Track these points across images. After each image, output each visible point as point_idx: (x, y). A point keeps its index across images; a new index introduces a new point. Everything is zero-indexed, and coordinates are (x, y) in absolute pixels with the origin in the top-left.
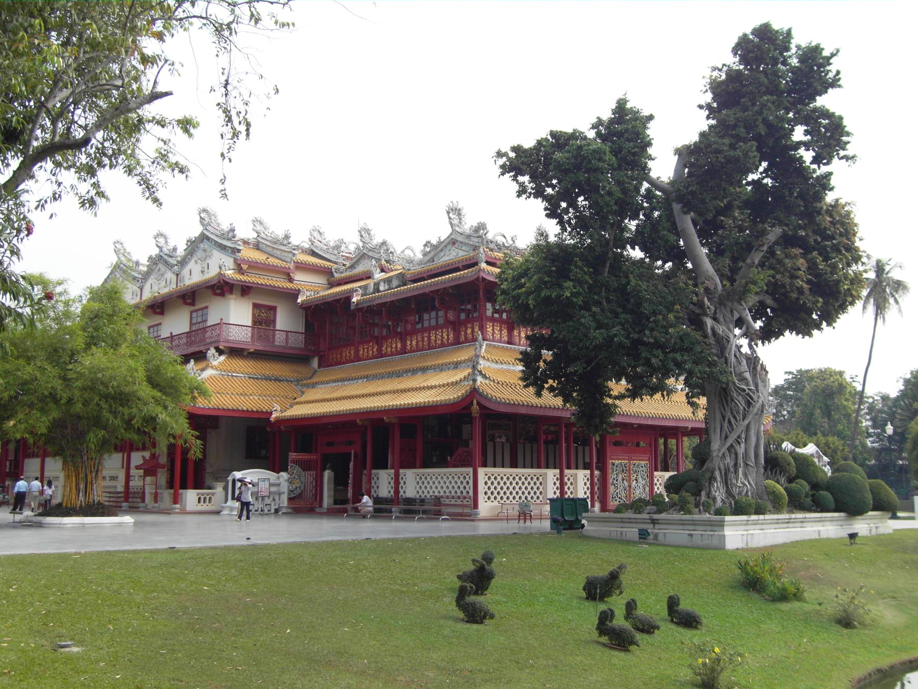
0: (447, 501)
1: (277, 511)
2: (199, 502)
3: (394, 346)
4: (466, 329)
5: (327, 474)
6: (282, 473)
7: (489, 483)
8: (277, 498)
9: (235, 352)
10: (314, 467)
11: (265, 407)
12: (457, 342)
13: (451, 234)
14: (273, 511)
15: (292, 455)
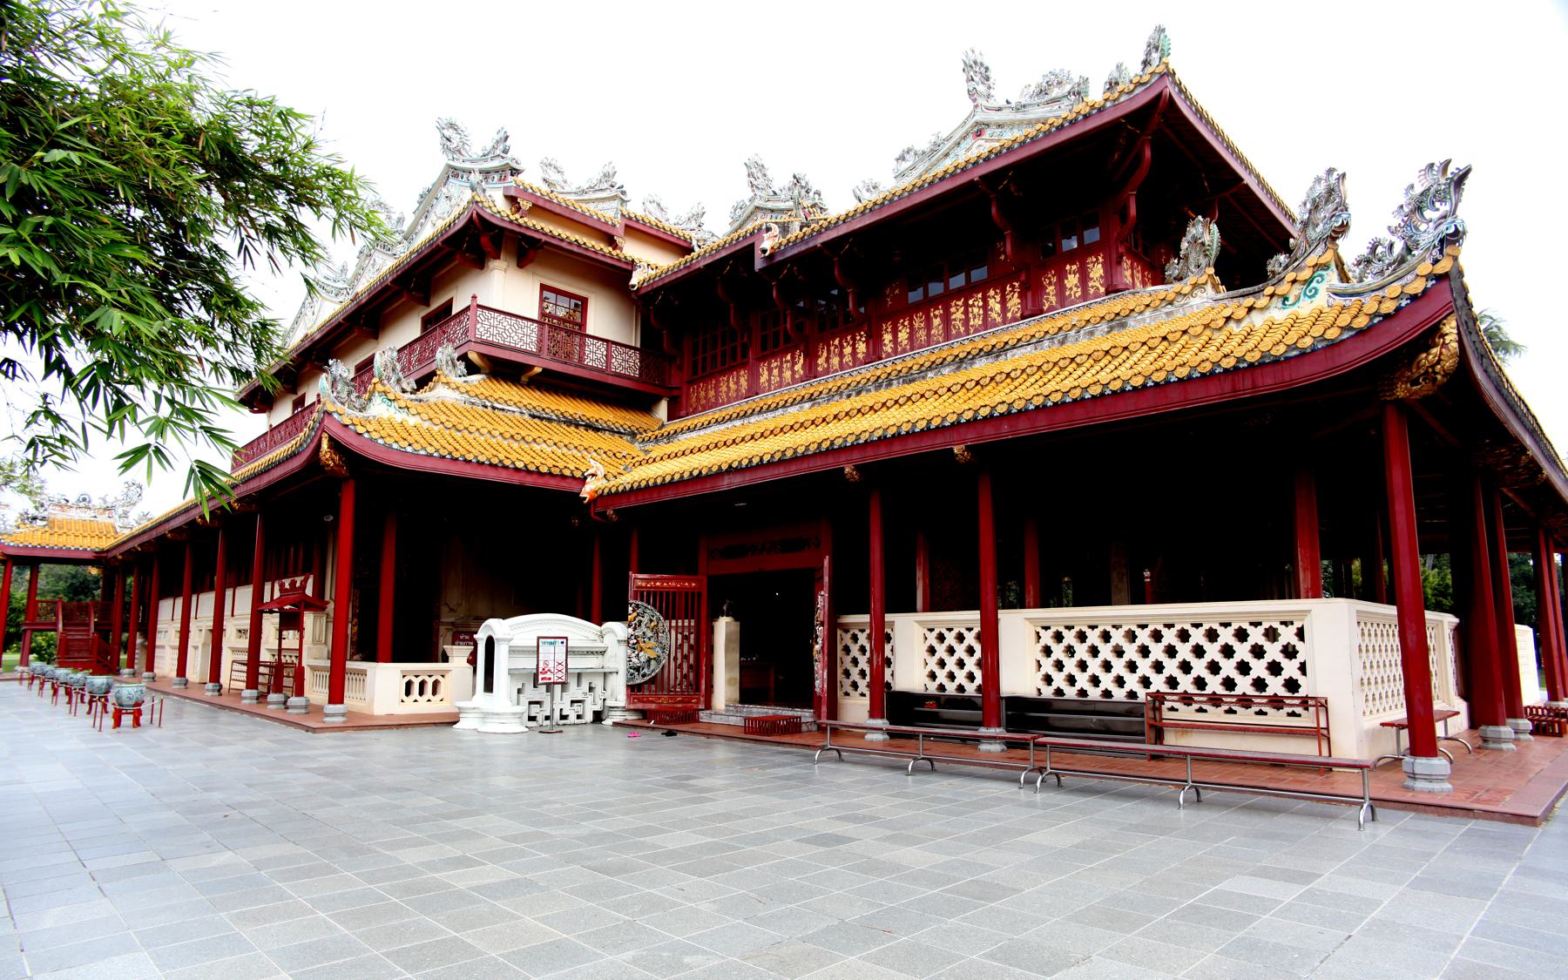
0: (1186, 713)
1: (598, 717)
2: (408, 693)
3: (848, 350)
5: (723, 628)
6: (609, 625)
7: (941, 651)
8: (598, 683)
9: (504, 369)
10: (694, 613)
11: (568, 463)
13: (973, 114)
14: (589, 717)
15: (638, 580)
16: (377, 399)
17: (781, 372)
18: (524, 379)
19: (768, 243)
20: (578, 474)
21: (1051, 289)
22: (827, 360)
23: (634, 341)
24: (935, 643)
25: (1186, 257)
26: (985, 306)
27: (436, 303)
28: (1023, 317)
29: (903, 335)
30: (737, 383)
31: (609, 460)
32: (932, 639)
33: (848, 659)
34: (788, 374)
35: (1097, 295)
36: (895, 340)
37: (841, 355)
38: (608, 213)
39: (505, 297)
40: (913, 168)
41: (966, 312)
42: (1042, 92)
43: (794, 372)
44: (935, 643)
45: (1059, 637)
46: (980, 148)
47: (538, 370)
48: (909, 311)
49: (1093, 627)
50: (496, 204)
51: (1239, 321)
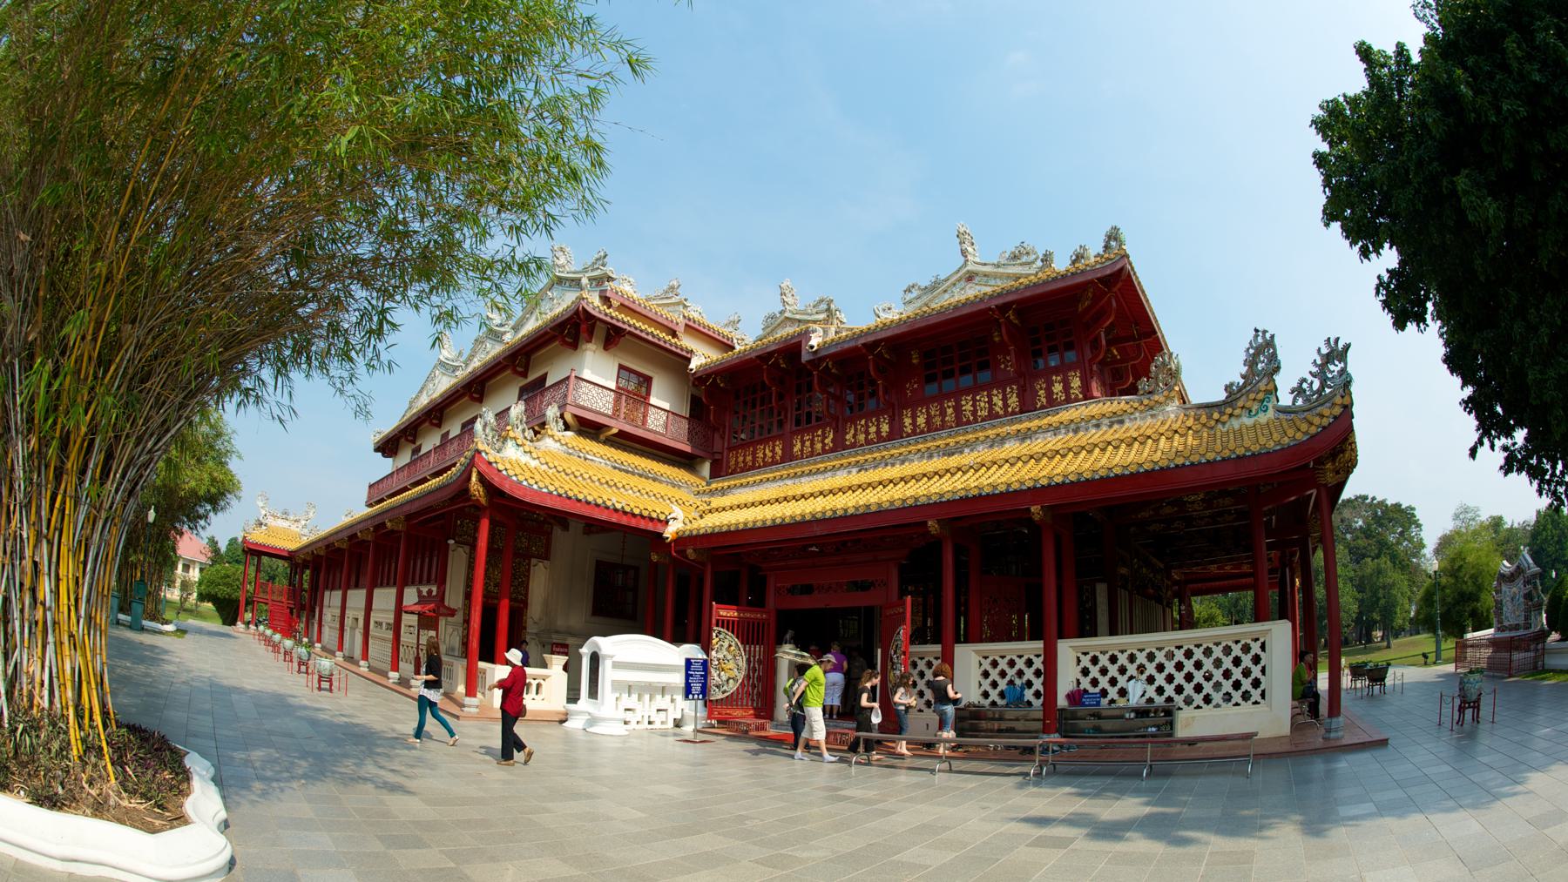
3: (873, 429)
4: (1050, 384)
9: (588, 428)
11: (653, 507)
12: (1027, 407)
16: (510, 443)
17: (812, 445)
18: (602, 437)
19: (815, 341)
20: (662, 517)
21: (1042, 392)
22: (855, 436)
23: (685, 412)
24: (989, 669)
25: (1157, 378)
26: (990, 402)
27: (532, 377)
28: (1021, 412)
29: (921, 420)
30: (773, 451)
31: (683, 506)
32: (986, 665)
33: (915, 672)
34: (819, 446)
35: (1077, 400)
36: (914, 423)
37: (867, 433)
38: (676, 317)
39: (594, 377)
40: (918, 298)
41: (974, 405)
42: (1015, 257)
43: (824, 445)
44: (989, 669)
45: (1095, 660)
46: (971, 292)
47: (615, 431)
48: (925, 402)
49: (1122, 652)
50: (593, 302)
51: (1224, 424)
